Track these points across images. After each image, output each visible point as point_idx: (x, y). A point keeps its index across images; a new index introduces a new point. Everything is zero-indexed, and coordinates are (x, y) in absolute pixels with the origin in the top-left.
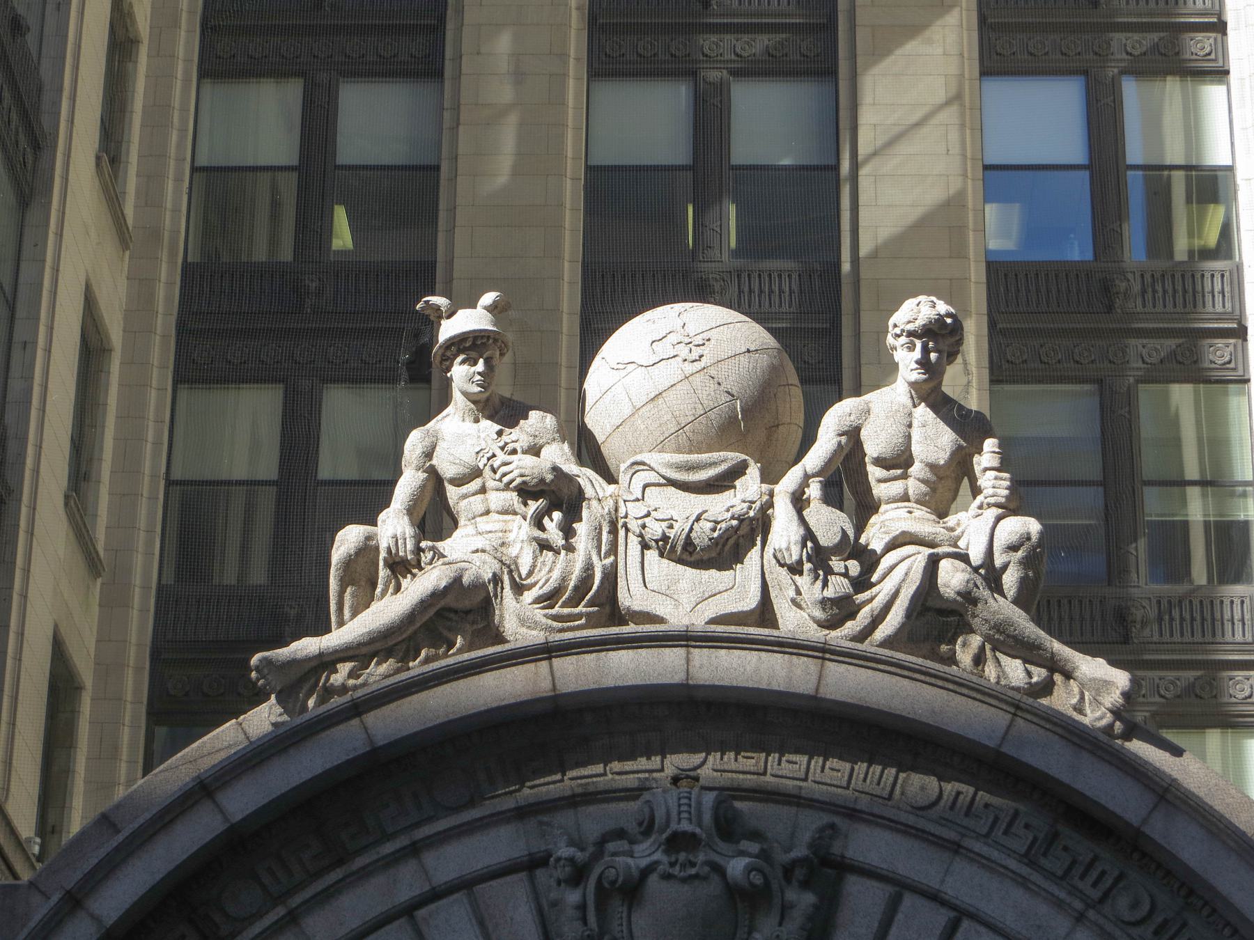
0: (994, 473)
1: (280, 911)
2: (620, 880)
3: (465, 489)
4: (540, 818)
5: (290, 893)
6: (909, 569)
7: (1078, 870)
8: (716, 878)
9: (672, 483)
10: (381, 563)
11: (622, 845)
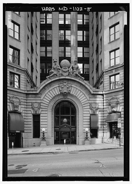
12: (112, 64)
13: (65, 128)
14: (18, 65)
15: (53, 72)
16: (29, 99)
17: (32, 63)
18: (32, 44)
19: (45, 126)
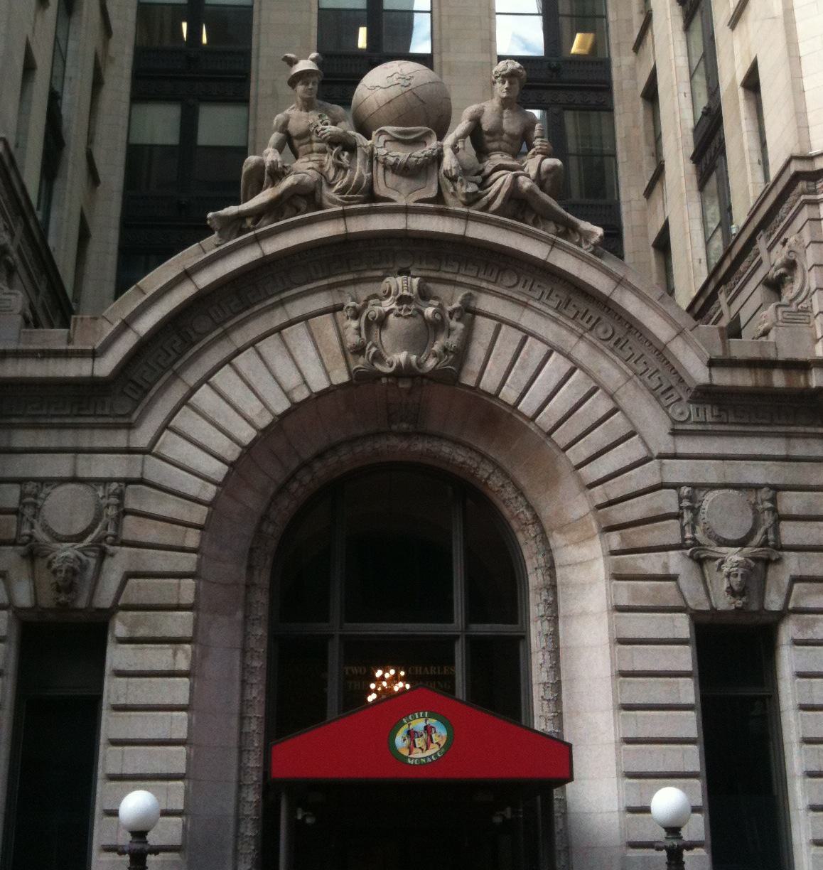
0: (540, 139)
1: (220, 330)
2: (377, 317)
3: (302, 142)
4: (338, 289)
5: (225, 322)
6: (505, 180)
7: (580, 315)
8: (419, 316)
9: (397, 140)
10: (266, 173)
11: (377, 301)
15: (277, 174)
17: (54, 98)
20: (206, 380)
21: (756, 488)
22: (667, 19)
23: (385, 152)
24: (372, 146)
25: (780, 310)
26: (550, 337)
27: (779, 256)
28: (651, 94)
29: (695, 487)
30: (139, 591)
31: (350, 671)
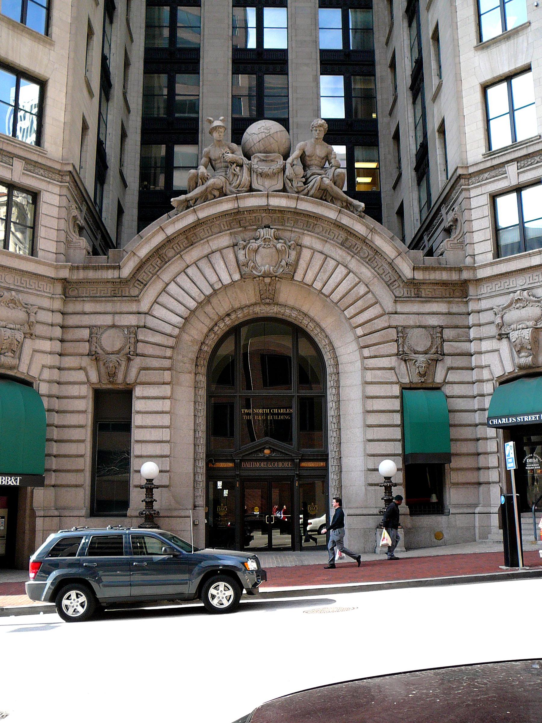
12: (501, 138)
13: (268, 459)
14: (38, 148)
15: (205, 179)
16: (78, 307)
18: (104, 59)
19: (156, 449)
20: (173, 280)
21: (434, 327)
22: (404, 98)
23: (257, 166)
24: (251, 164)
25: (449, 243)
26: (337, 258)
27: (450, 217)
28: (396, 137)
29: (404, 327)
30: (145, 376)
31: (244, 411)
